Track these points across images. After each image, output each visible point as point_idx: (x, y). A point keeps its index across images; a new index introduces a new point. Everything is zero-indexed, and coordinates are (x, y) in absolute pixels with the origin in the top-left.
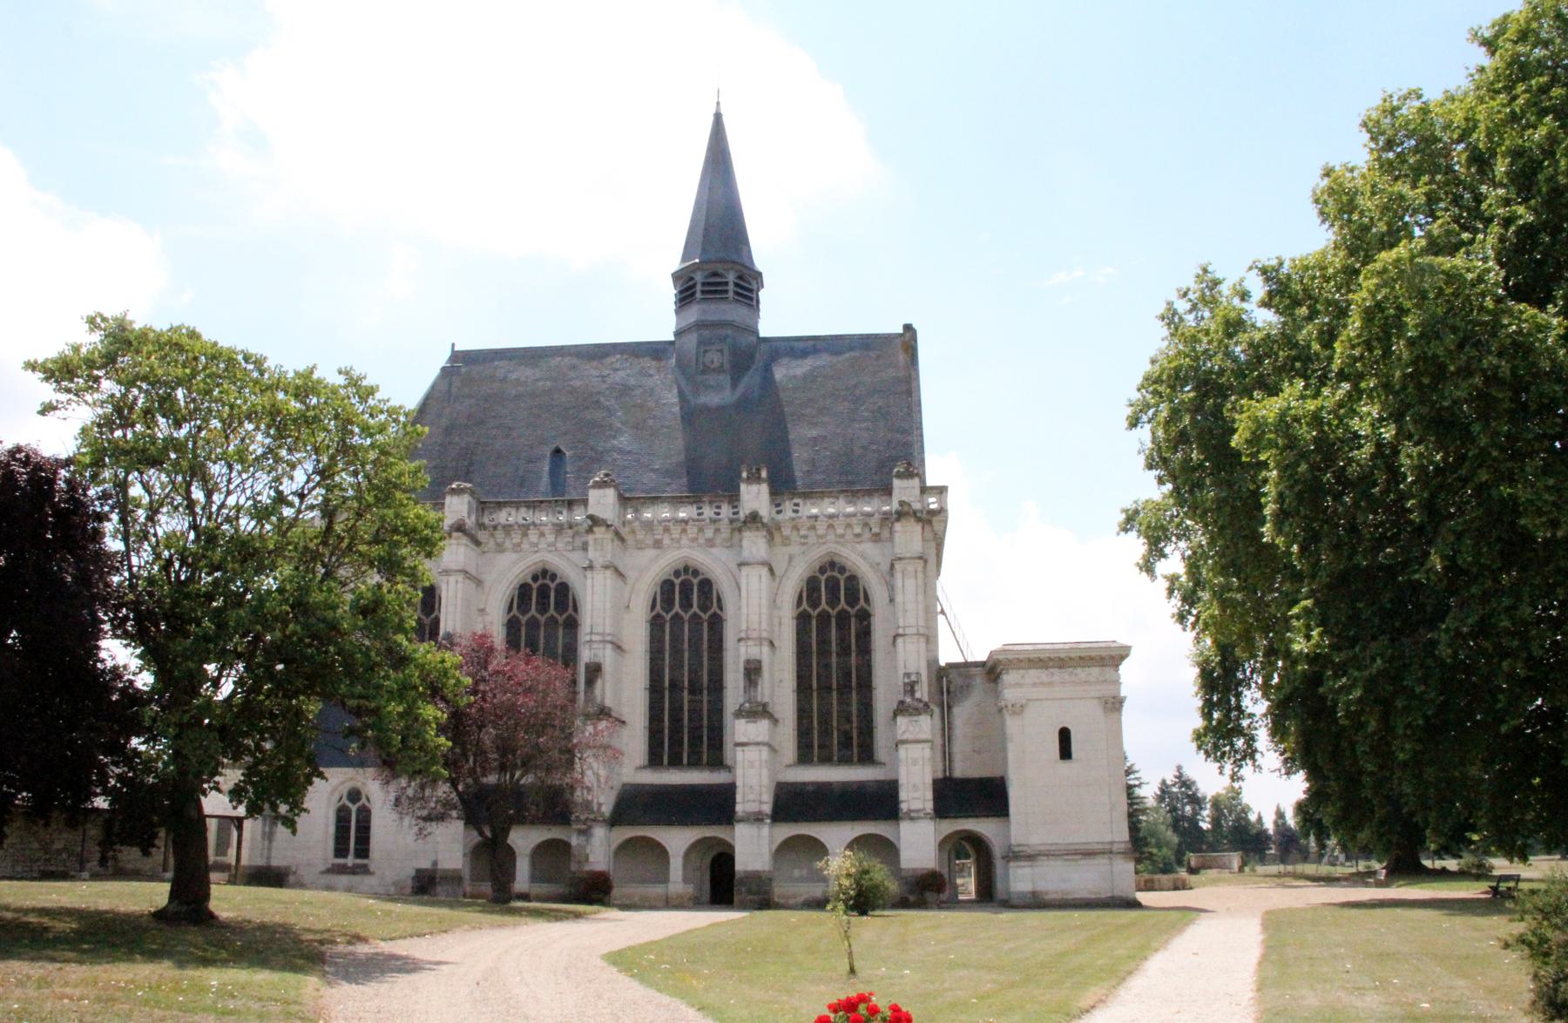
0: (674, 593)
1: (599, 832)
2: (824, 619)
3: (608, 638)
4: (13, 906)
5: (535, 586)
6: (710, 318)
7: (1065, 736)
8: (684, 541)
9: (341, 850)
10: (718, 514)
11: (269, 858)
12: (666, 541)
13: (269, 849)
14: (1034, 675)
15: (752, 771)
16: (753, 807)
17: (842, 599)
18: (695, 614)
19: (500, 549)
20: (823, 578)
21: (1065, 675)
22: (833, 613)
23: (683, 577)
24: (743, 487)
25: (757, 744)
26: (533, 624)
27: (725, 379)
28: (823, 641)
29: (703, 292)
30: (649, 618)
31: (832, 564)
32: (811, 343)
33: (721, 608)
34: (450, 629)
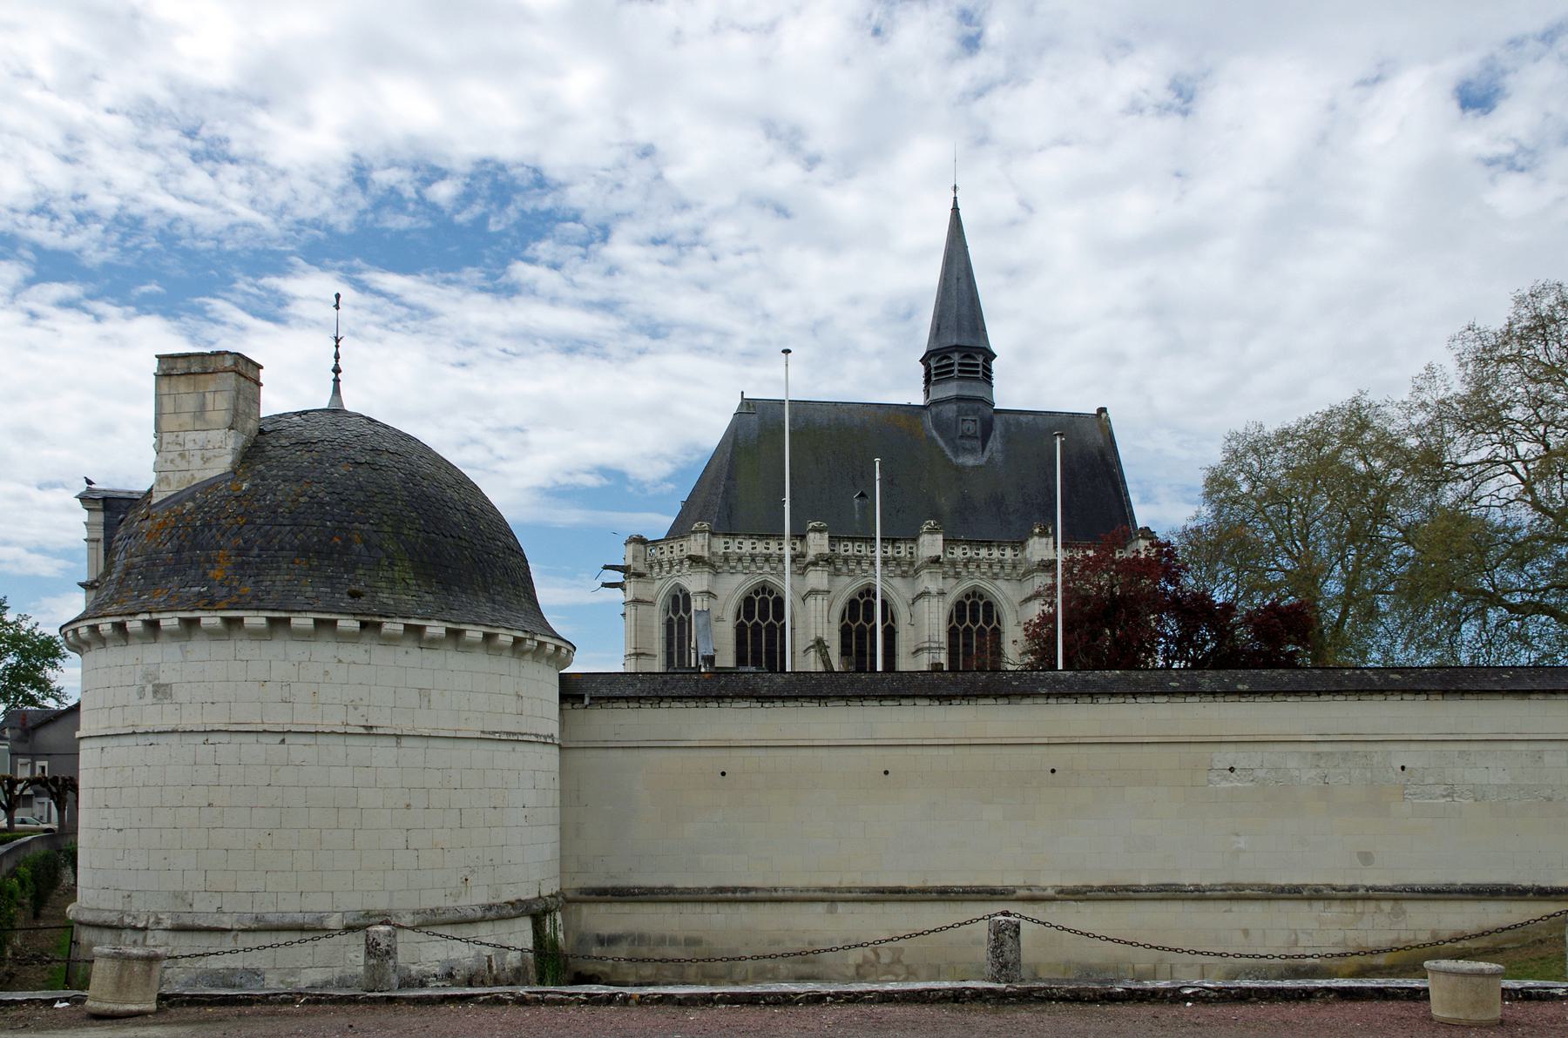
0: (966, 612)
6: (967, 393)
8: (767, 569)
10: (1003, 555)
12: (964, 573)
17: (771, 615)
18: (756, 623)
23: (865, 598)
26: (968, 630)
27: (977, 444)
28: (967, 645)
29: (960, 371)
30: (665, 621)
32: (1031, 417)
33: (893, 620)
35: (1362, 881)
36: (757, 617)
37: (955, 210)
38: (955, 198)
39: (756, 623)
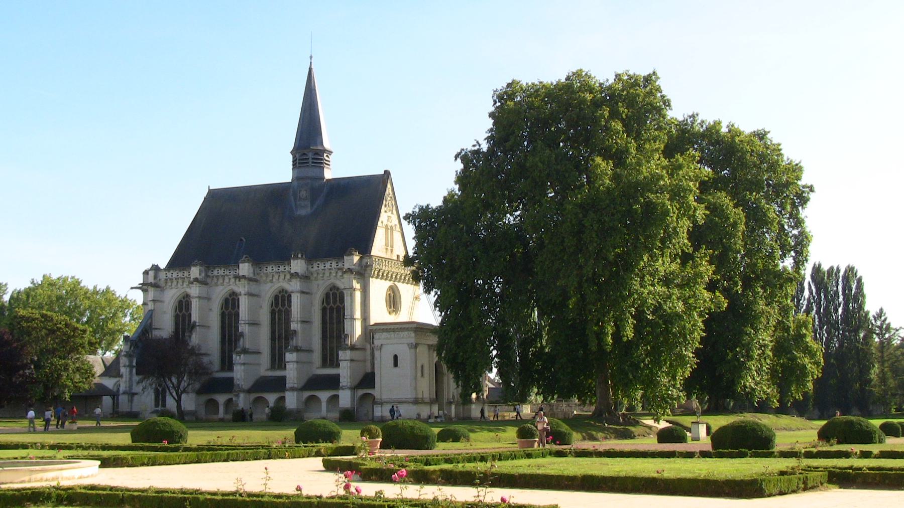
1: (242, 395)
2: (332, 309)
3: (247, 322)
4: (838, 467)
5: (230, 299)
7: (396, 357)
9: (157, 405)
11: (131, 408)
13: (131, 406)
14: (385, 335)
15: (292, 372)
16: (291, 385)
19: (216, 285)
20: (331, 293)
21: (392, 334)
22: (335, 307)
24: (292, 261)
25: (292, 362)
27: (308, 203)
28: (331, 318)
30: (270, 311)
31: (334, 287)
34: (195, 320)
35: (579, 460)
36: (280, 306)
37: (310, 69)
38: (311, 63)
39: (230, 312)
